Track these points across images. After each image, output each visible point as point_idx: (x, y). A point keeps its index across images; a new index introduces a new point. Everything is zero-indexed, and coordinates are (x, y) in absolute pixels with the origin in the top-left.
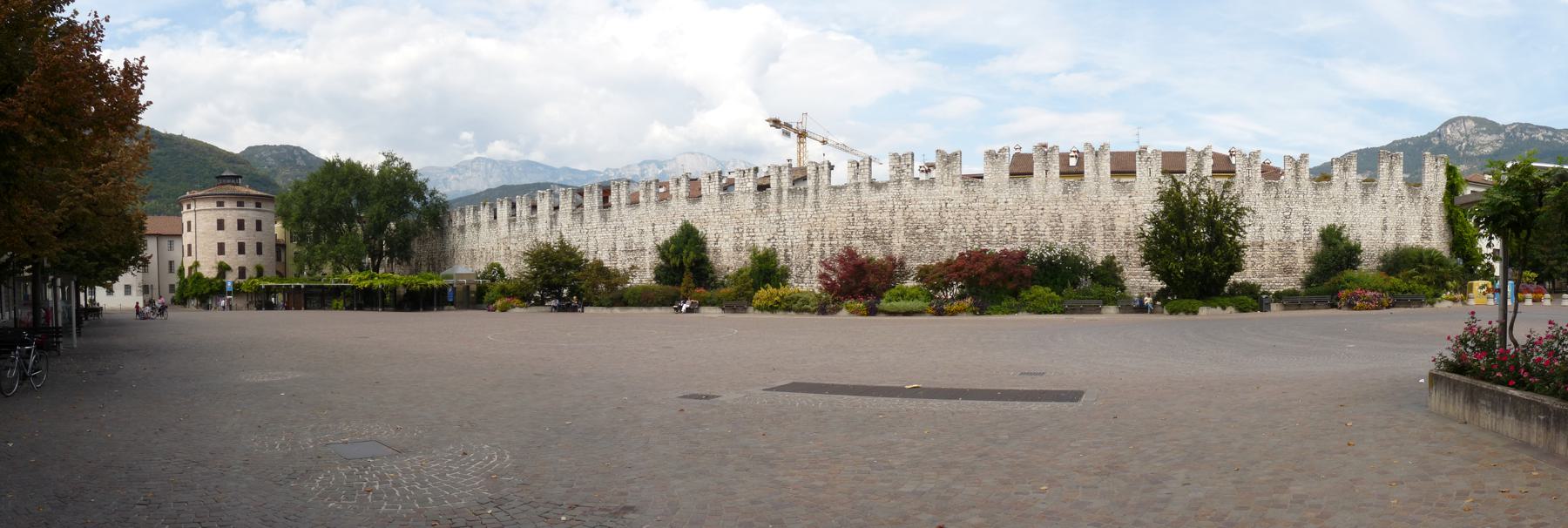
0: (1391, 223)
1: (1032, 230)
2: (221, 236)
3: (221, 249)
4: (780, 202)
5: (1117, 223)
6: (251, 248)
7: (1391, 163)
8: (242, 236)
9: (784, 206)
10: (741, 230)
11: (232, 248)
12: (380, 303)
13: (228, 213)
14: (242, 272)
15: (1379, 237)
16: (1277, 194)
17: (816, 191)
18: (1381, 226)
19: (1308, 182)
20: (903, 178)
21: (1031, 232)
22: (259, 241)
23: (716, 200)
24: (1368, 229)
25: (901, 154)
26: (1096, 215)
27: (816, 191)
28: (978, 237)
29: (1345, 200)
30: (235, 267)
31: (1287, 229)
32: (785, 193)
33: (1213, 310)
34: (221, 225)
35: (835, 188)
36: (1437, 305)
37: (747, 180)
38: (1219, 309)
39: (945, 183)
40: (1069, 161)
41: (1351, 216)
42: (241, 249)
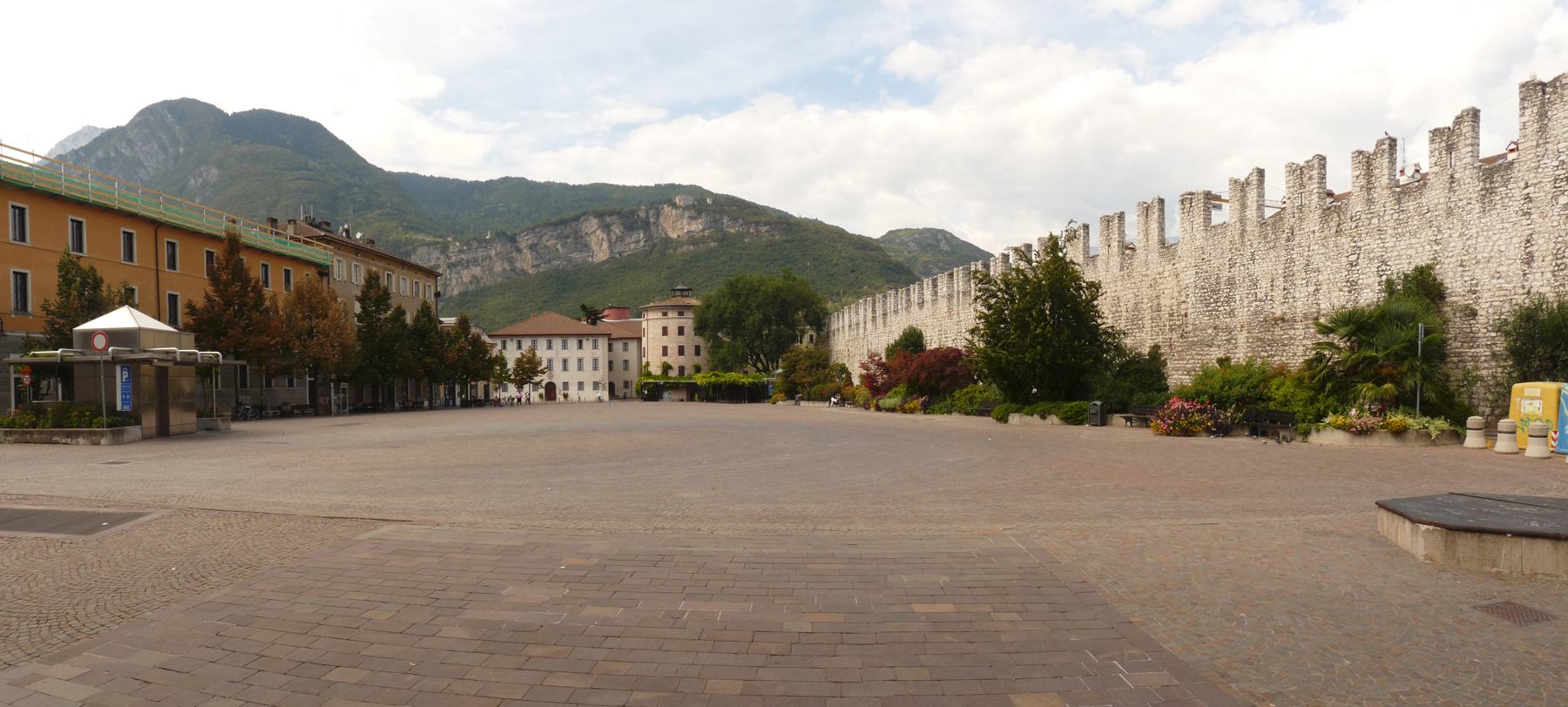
0: (1542, 246)
2: (665, 340)
3: (665, 351)
5: (1163, 302)
6: (689, 350)
7: (1543, 105)
8: (682, 340)
11: (673, 350)
13: (670, 321)
14: (682, 369)
15: (1517, 281)
16: (1339, 225)
18: (1521, 253)
19: (1386, 192)
22: (698, 344)
23: (930, 305)
24: (1493, 265)
26: (1146, 292)
29: (1450, 212)
30: (675, 367)
31: (1353, 285)
32: (961, 295)
33: (1028, 418)
34: (665, 331)
36: (1315, 438)
38: (1036, 417)
40: (1528, 457)
41: (1460, 244)
42: (681, 351)
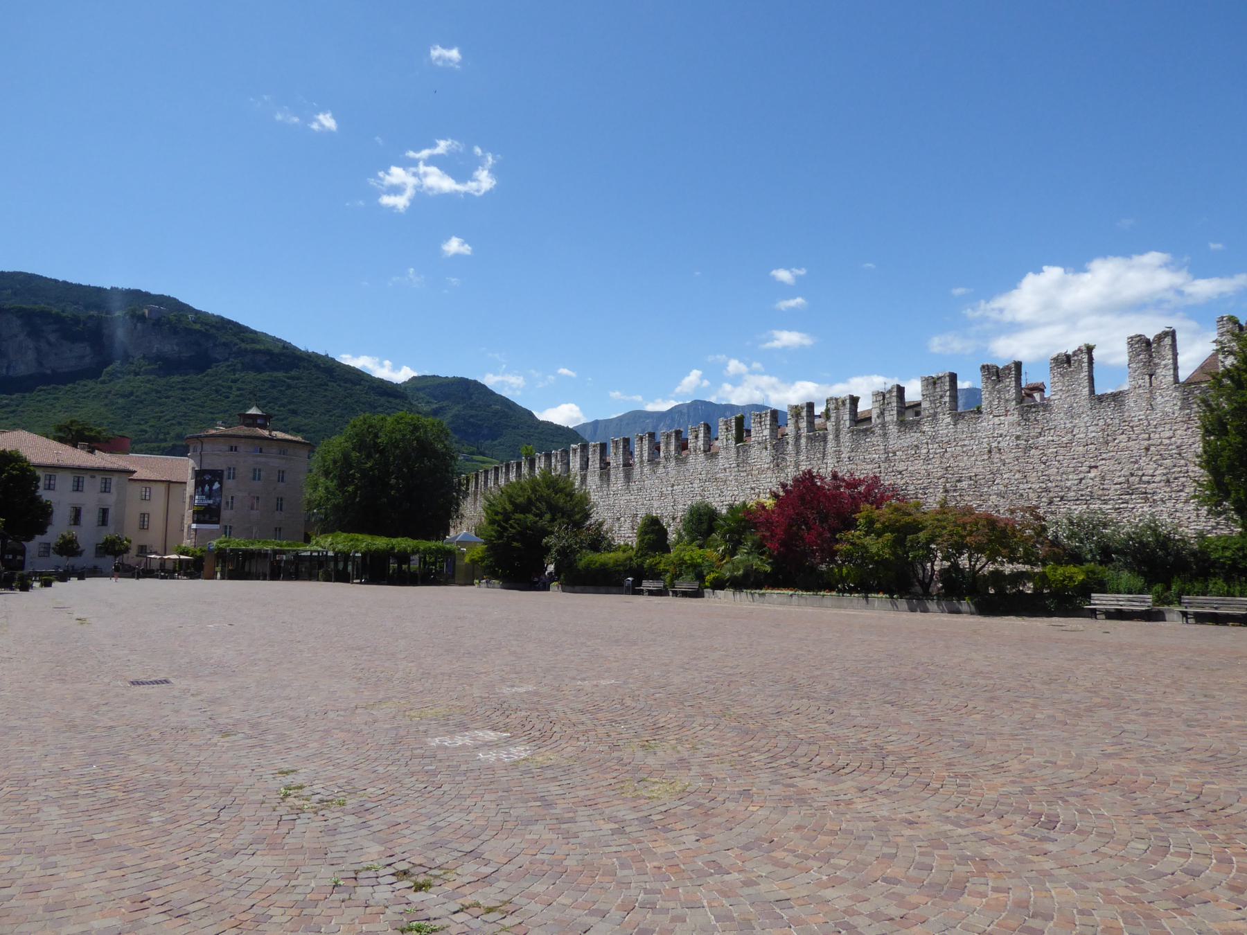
1: (1132, 475)
4: (798, 453)
9: (802, 458)
10: (757, 490)
12: (184, 564)
17: (837, 436)
20: (939, 410)
21: (1131, 479)
25: (1151, 337)
27: (837, 436)
28: (1047, 490)
32: (803, 441)
35: (1101, 399)
37: (763, 427)
39: (996, 412)
